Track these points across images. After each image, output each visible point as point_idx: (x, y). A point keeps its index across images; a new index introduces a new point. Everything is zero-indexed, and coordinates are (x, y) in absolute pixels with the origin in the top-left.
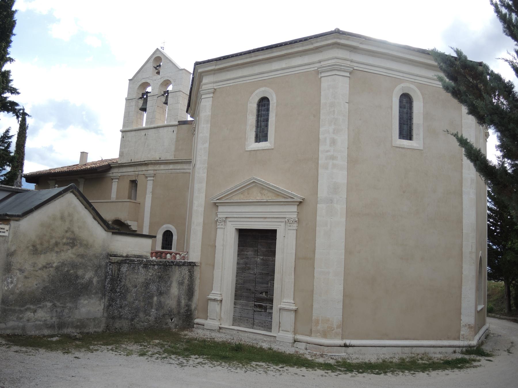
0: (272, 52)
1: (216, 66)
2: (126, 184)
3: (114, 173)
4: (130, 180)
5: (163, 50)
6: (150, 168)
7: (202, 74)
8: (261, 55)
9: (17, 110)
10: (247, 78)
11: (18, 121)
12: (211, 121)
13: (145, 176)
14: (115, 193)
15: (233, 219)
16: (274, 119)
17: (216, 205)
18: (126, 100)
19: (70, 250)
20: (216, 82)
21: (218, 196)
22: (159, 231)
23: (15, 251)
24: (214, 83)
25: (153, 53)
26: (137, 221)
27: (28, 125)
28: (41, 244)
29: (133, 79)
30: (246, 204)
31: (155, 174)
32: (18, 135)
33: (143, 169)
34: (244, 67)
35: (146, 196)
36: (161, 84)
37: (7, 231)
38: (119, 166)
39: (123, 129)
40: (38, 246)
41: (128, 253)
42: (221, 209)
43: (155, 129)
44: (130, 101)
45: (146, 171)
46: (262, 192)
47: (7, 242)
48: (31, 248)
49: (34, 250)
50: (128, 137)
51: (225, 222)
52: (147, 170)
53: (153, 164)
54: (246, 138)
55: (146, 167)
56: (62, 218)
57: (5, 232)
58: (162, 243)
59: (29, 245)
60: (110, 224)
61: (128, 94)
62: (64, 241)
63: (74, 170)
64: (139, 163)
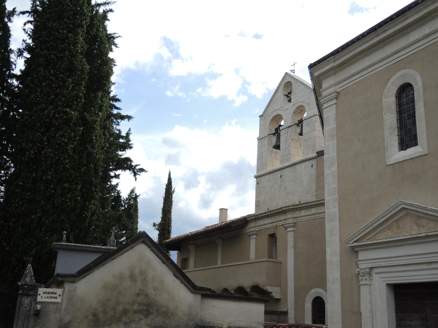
0: (407, 18)
1: (334, 62)
2: (265, 239)
3: (252, 227)
4: (269, 235)
5: (294, 73)
6: (289, 215)
7: (321, 78)
8: (392, 27)
9: (133, 167)
10: (377, 66)
11: (135, 178)
12: (337, 135)
13: (284, 226)
14: (254, 252)
15: (381, 270)
16: (422, 110)
17: (354, 251)
18: (258, 140)
19: (143, 319)
20: (339, 83)
21: (354, 236)
22: (307, 298)
23: (70, 322)
24: (336, 85)
25: (282, 80)
26: (280, 286)
27: (174, 189)
28: (105, 312)
29: (264, 115)
30: (397, 244)
31: (295, 223)
32: (164, 201)
33: (282, 219)
34: (371, 53)
35: (288, 252)
36: (294, 112)
37: (60, 296)
38: (255, 218)
39: (257, 173)
40: (100, 315)
41: (230, 324)
42: (362, 255)
43: (291, 168)
44: (262, 140)
45: (284, 220)
46: (418, 222)
47: (60, 310)
48: (91, 317)
49: (94, 321)
50: (263, 182)
51: (370, 275)
52: (286, 220)
53: (292, 211)
54: (386, 146)
55: (284, 216)
56: (132, 277)
57: (57, 297)
58: (312, 315)
59: (88, 313)
60: (248, 291)
61: (260, 132)
62: (135, 307)
63: (209, 229)
64: (276, 212)
